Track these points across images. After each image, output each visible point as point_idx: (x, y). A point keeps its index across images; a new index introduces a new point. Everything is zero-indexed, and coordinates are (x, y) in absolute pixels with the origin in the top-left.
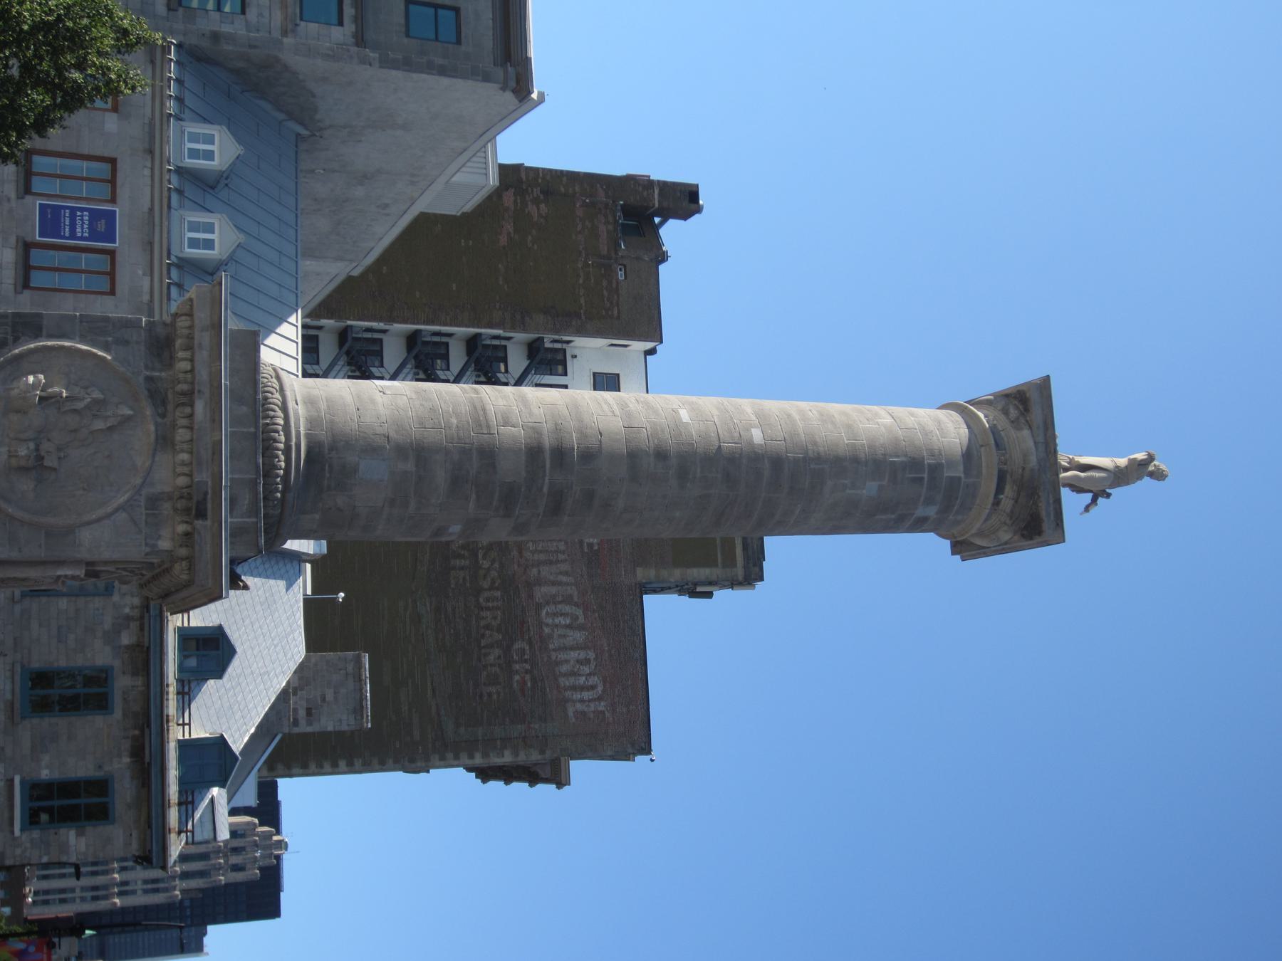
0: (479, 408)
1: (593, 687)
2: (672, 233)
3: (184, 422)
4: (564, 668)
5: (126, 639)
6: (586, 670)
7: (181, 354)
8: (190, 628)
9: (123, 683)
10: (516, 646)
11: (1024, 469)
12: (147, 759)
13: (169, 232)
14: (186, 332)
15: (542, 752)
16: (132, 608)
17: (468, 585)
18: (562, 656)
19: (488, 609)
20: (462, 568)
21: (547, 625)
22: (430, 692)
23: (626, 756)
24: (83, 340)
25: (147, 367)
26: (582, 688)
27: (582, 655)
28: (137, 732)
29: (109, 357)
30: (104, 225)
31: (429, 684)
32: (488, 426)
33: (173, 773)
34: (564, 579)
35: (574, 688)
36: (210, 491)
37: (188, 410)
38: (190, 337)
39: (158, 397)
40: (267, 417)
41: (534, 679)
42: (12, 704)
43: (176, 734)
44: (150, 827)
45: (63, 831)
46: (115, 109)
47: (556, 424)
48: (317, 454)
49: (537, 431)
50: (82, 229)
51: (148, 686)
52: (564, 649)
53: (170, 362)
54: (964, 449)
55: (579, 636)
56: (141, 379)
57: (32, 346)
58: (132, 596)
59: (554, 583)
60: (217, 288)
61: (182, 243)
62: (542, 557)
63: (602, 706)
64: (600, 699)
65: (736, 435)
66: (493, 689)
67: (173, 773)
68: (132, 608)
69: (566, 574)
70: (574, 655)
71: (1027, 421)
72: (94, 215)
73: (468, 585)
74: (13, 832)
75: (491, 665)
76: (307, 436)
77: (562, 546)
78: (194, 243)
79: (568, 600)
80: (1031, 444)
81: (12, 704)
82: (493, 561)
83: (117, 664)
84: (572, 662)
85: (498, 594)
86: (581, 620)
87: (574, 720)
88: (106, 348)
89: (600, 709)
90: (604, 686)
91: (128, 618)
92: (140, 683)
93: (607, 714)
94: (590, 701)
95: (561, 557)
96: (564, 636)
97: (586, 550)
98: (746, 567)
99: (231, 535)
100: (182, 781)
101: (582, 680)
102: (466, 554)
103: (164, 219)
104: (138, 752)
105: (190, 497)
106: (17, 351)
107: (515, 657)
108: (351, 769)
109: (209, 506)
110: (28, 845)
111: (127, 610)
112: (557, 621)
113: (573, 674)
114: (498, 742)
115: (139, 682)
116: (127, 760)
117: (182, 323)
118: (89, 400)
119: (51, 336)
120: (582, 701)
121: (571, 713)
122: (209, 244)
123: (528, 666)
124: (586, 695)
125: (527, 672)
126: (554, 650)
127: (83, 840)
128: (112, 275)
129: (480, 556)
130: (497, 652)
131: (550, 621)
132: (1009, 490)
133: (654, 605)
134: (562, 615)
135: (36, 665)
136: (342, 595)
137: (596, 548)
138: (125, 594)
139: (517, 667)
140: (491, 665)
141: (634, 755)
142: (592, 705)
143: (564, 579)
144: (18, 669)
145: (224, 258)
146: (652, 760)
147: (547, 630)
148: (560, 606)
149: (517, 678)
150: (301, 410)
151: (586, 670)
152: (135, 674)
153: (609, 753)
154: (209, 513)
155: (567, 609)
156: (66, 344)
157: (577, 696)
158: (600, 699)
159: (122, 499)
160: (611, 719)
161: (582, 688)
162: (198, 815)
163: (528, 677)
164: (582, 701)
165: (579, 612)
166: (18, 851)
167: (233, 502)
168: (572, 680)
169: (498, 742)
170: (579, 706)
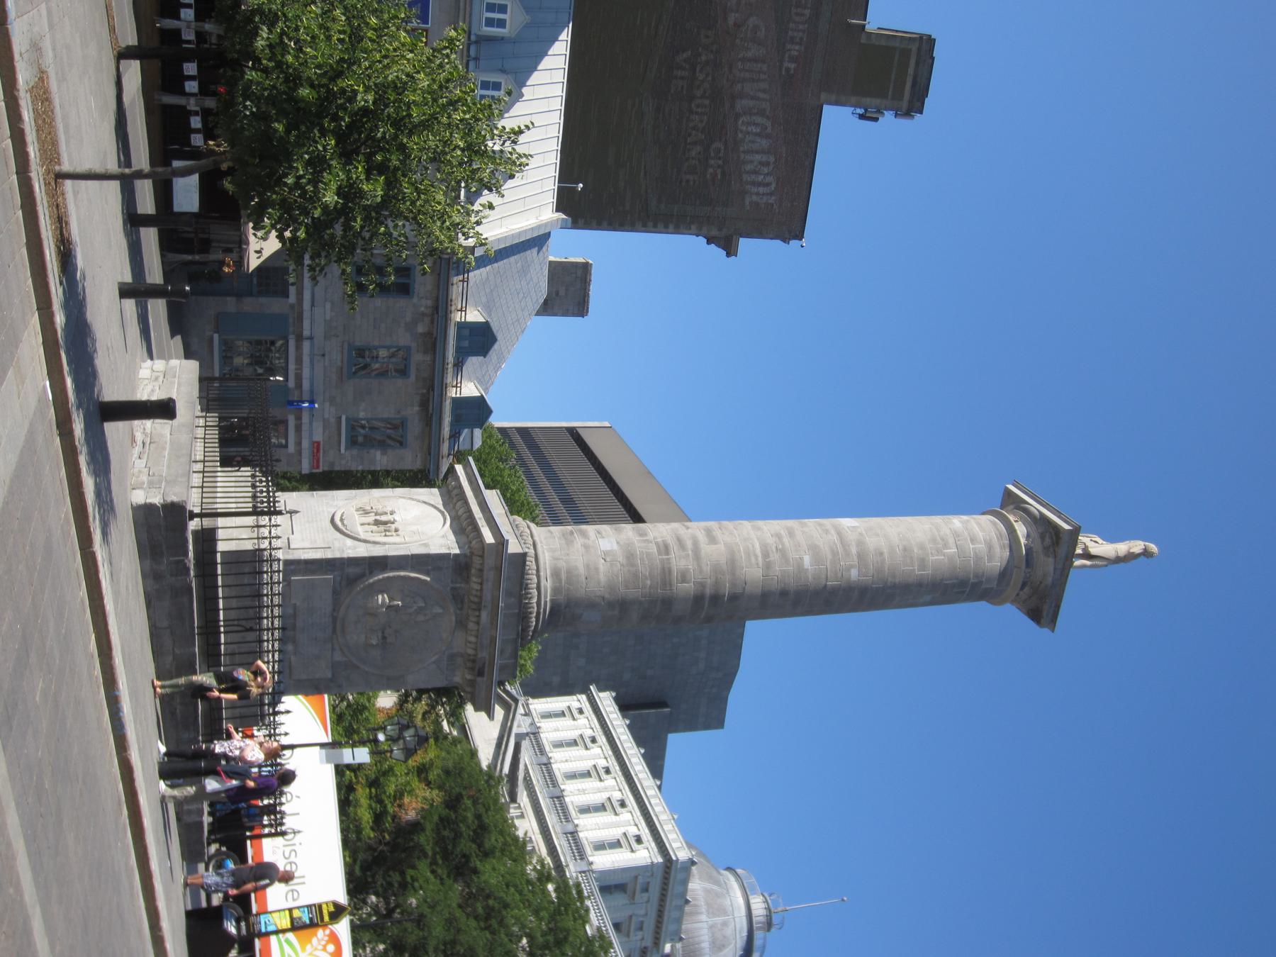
0: (667, 570)
1: (768, 185)
3: (474, 619)
4: (749, 167)
6: (766, 170)
7: (474, 579)
8: (465, 323)
9: (418, 358)
10: (714, 146)
11: (1041, 582)
12: (431, 411)
13: (471, 15)
14: (478, 567)
15: (720, 230)
16: (426, 307)
17: (685, 92)
18: (749, 157)
19: (697, 113)
20: (682, 78)
21: (741, 132)
22: (642, 174)
23: (785, 240)
24: (413, 570)
25: (452, 582)
26: (760, 184)
27: (764, 158)
28: (425, 391)
29: (428, 579)
31: (643, 167)
32: (671, 585)
33: (447, 419)
34: (761, 95)
35: (754, 184)
36: (487, 663)
37: (477, 613)
38: (481, 570)
40: (526, 598)
41: (723, 174)
42: (342, 368)
43: (453, 393)
44: (430, 454)
45: (372, 451)
47: (717, 578)
48: (556, 610)
49: (703, 585)
51: (434, 361)
52: (751, 152)
53: (467, 580)
54: (1002, 569)
55: (764, 143)
56: (448, 589)
57: (381, 577)
58: (427, 299)
59: (753, 98)
60: (501, 546)
61: (480, 23)
62: (747, 75)
63: (772, 200)
64: (771, 194)
65: (840, 575)
66: (691, 177)
67: (447, 419)
68: (426, 307)
69: (764, 91)
70: (758, 157)
71: (1054, 551)
73: (685, 92)
74: (340, 451)
75: (693, 158)
76: (552, 601)
77: (765, 68)
78: (490, 22)
79: (761, 113)
80: (1051, 568)
81: (342, 368)
82: (707, 75)
83: (414, 345)
84: (755, 163)
85: (707, 102)
86: (769, 130)
87: (748, 208)
88: (427, 574)
89: (770, 201)
90: (777, 184)
91: (423, 314)
92: (428, 359)
93: (775, 206)
94: (763, 194)
95: (762, 77)
96: (753, 142)
97: (783, 73)
98: (911, 102)
99: (500, 670)
100: (452, 424)
102: (687, 66)
103: (467, 6)
104: (424, 404)
105: (474, 661)
106: (371, 581)
107: (712, 154)
109: (486, 669)
110: (350, 458)
111: (422, 309)
112: (750, 129)
113: (756, 172)
114: (688, 218)
115: (428, 358)
116: (417, 408)
117: (476, 560)
118: (415, 608)
119: (393, 569)
120: (757, 194)
121: (747, 202)
122: (501, 24)
123: (720, 162)
124: (761, 190)
125: (719, 166)
126: (744, 152)
127: (385, 458)
129: (698, 70)
130: (699, 148)
131: (744, 128)
132: (1026, 590)
134: (754, 124)
135: (358, 344)
136: (581, 185)
137: (792, 72)
138: (422, 298)
139: (712, 162)
140: (693, 158)
141: (790, 239)
142: (765, 198)
143: (761, 95)
144: (346, 346)
145: (513, 36)
146: (802, 246)
147: (740, 135)
148: (754, 118)
149: (711, 170)
150: (547, 585)
151: (766, 170)
152: (425, 352)
153: (771, 236)
154: (486, 674)
155: (759, 120)
156: (402, 574)
157: (754, 190)
158: (771, 194)
159: (433, 659)
160: (777, 211)
161: (760, 184)
162: (461, 439)
163: (719, 171)
164: (757, 194)
165: (769, 124)
166: (343, 462)
167: (502, 651)
168: (753, 177)
169: (688, 218)
170: (755, 198)
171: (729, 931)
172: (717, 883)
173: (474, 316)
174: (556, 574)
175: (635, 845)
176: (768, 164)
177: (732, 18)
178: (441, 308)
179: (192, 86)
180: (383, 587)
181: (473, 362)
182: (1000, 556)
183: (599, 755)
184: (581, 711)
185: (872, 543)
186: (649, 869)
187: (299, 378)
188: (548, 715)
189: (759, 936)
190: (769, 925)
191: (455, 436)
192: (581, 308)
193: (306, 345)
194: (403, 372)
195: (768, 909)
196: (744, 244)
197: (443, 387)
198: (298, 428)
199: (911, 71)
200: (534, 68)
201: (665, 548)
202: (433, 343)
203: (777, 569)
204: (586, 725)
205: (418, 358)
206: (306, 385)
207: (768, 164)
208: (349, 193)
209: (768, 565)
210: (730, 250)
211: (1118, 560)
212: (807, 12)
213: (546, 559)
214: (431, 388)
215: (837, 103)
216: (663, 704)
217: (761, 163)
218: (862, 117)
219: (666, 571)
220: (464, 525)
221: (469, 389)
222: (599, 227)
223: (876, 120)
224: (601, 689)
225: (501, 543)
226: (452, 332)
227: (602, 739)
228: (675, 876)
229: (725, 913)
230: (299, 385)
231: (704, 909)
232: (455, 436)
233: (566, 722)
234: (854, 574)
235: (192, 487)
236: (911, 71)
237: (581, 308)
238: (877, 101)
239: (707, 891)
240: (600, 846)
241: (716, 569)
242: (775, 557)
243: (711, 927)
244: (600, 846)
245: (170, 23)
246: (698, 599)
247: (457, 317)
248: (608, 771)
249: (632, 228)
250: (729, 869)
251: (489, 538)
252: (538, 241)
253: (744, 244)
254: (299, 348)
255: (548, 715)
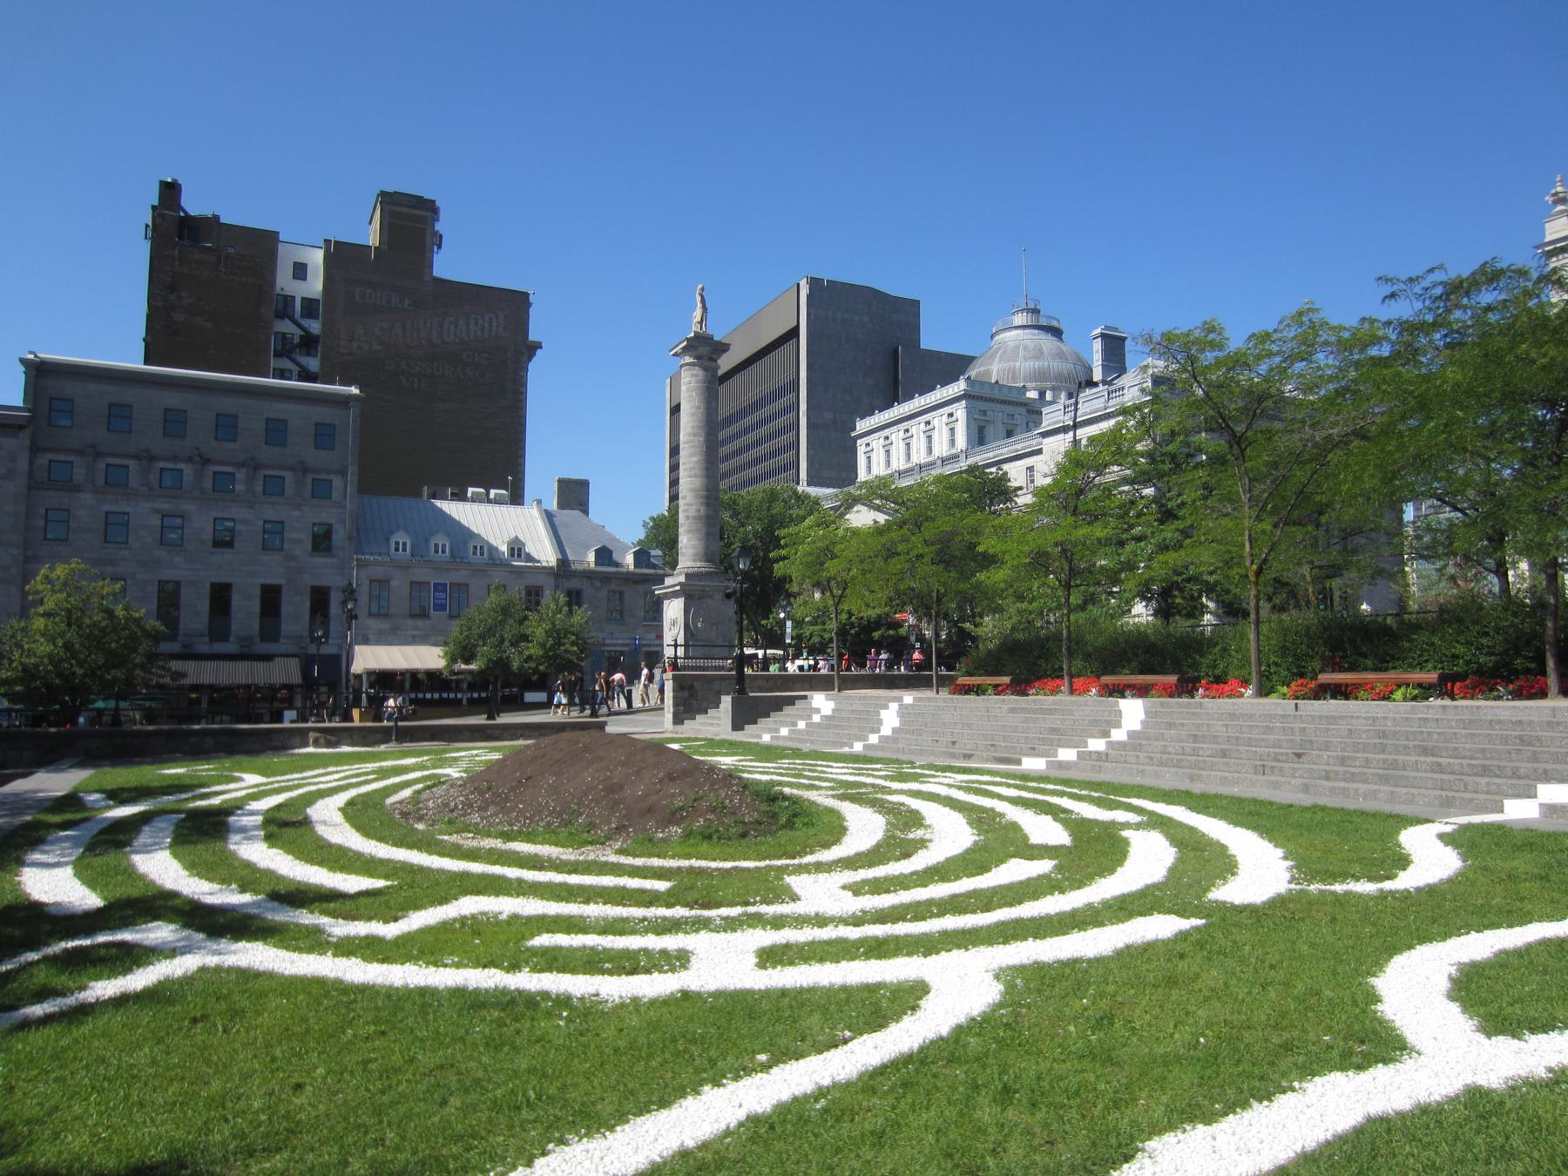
2: (193, 204)
4: (479, 334)
5: (599, 584)
9: (613, 586)
23: (529, 305)
26: (491, 326)
30: (440, 587)
35: (490, 330)
39: (701, 598)
46: (388, 582)
48: (708, 560)
50: (442, 595)
55: (462, 322)
70: (472, 327)
72: (435, 591)
78: (443, 551)
101: (486, 325)
104: (637, 582)
108: (523, 456)
124: (494, 324)
128: (459, 585)
133: (439, 271)
150: (698, 564)
151: (481, 321)
157: (494, 329)
171: (1031, 345)
172: (999, 349)
173: (591, 557)
174: (694, 560)
175: (954, 418)
176: (476, 319)
177: (376, 347)
178: (588, 575)
179: (459, 696)
180: (695, 624)
181: (615, 557)
182: (698, 371)
183: (896, 435)
184: (868, 445)
185: (689, 430)
186: (969, 410)
187: (624, 645)
188: (869, 469)
189: (1043, 322)
190: (1035, 311)
191: (654, 566)
192: (583, 485)
193: (608, 641)
194: (621, 594)
195: (1022, 311)
196: (533, 336)
197: (629, 573)
198: (649, 645)
199: (405, 210)
200: (459, 523)
201: (687, 517)
202: (605, 578)
203: (698, 472)
204: (876, 442)
205: (613, 586)
206: (627, 642)
207: (476, 319)
208: (573, 644)
209: (696, 476)
210: (538, 346)
211: (704, 308)
212: (368, 291)
213: (689, 564)
214: (628, 579)
215: (431, 266)
216: (896, 350)
217: (476, 323)
218: (440, 247)
219: (695, 518)
220: (675, 595)
221: (629, 560)
222: (524, 440)
223: (441, 236)
224: (854, 429)
225: (680, 584)
226: (601, 569)
227: (886, 432)
228: (977, 391)
229: (1018, 347)
230: (627, 645)
231: (1012, 364)
232: (654, 566)
233: (874, 455)
234: (701, 439)
235: (49, 479)
236: (405, 210)
237: (583, 485)
238: (428, 236)
239: (1000, 361)
240: (952, 442)
241: (696, 497)
242: (693, 472)
243: (1025, 359)
244: (952, 442)
245: (465, 702)
246: (707, 505)
247: (592, 565)
248: (907, 431)
249: (524, 417)
250: (992, 337)
251: (678, 588)
252: (549, 517)
253: (533, 336)
254: (608, 645)
255: (869, 469)
